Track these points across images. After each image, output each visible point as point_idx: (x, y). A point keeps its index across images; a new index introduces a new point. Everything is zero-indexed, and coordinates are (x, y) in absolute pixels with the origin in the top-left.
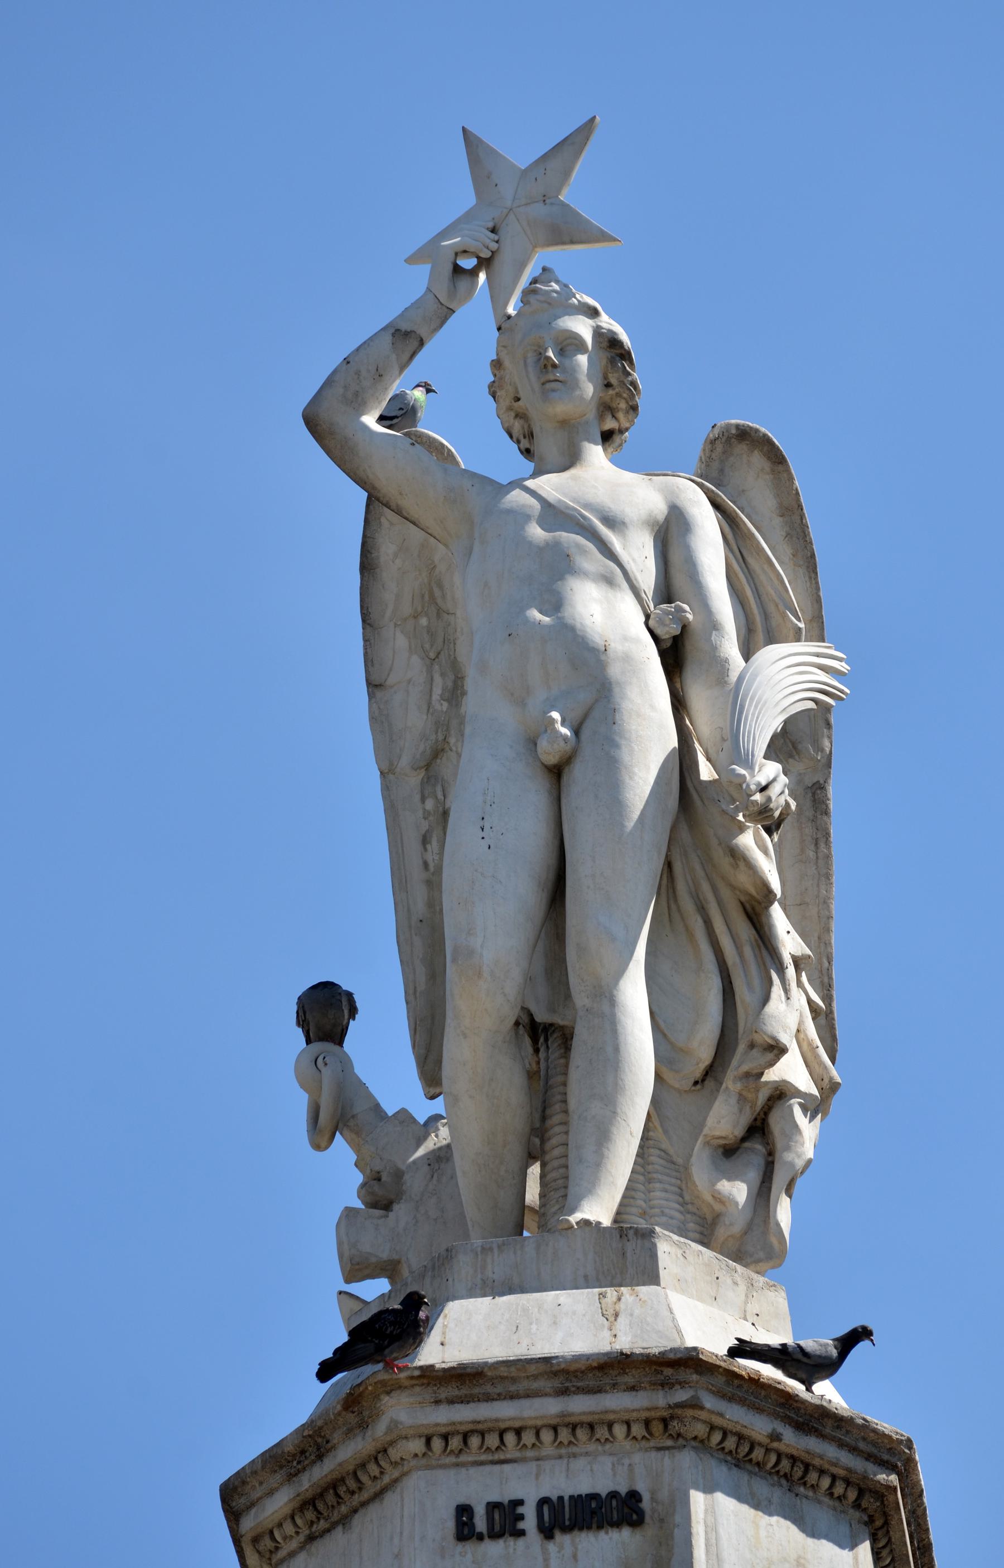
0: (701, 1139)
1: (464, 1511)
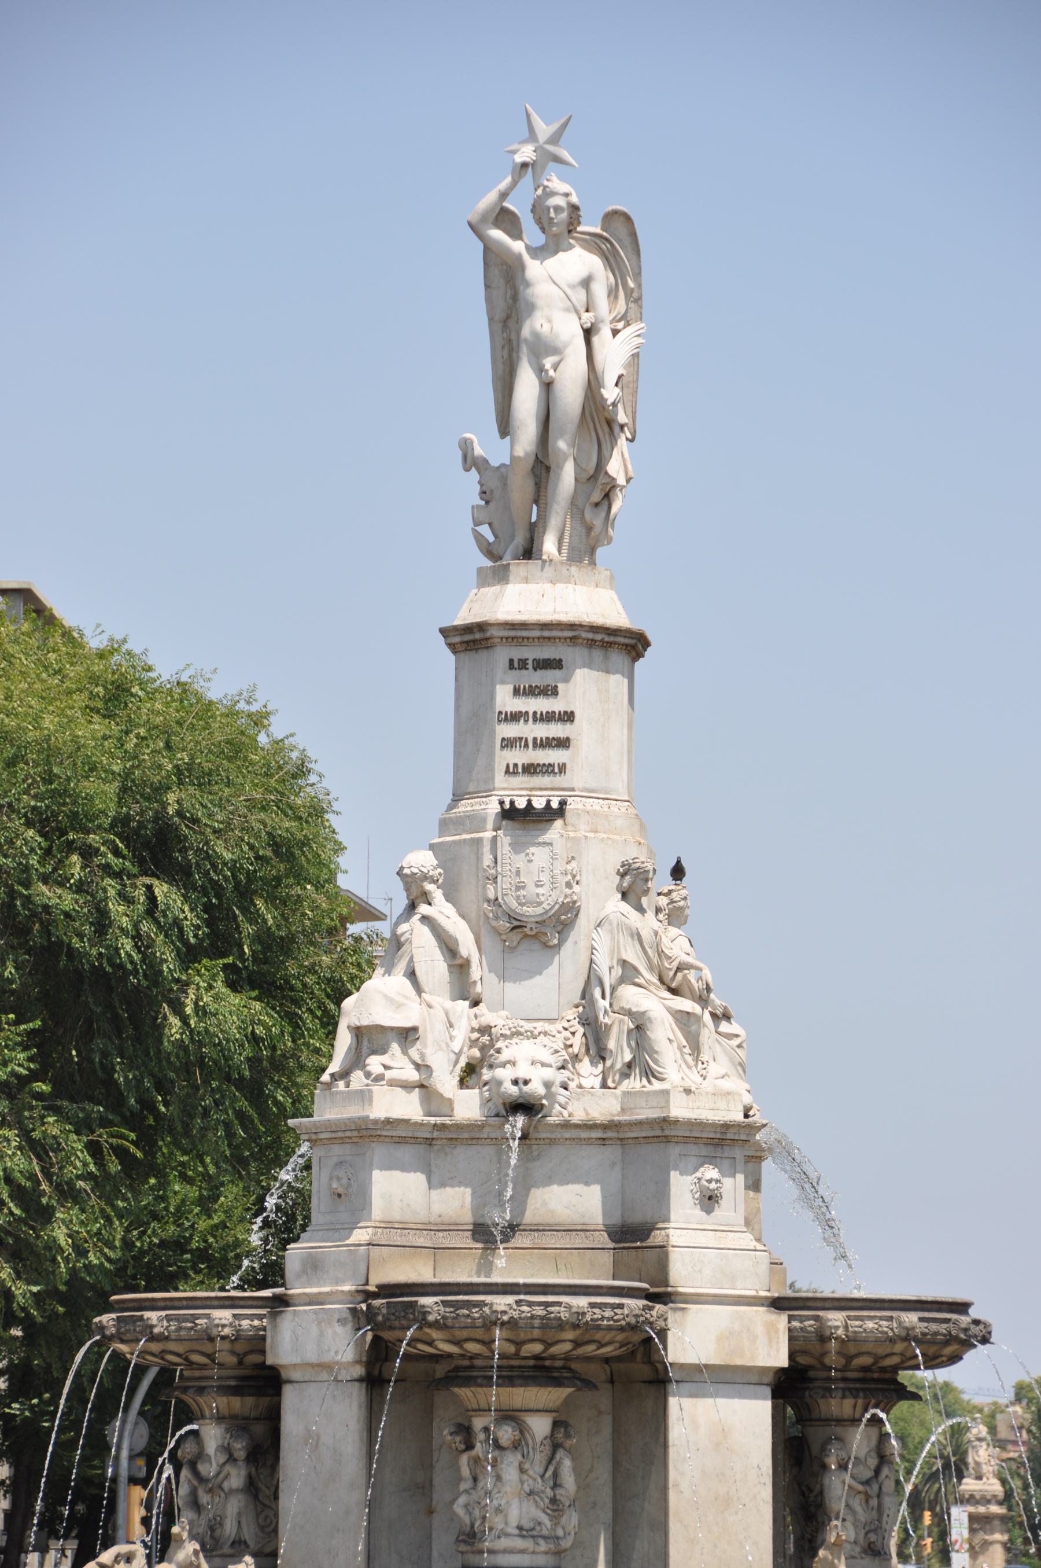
1: (511, 661)
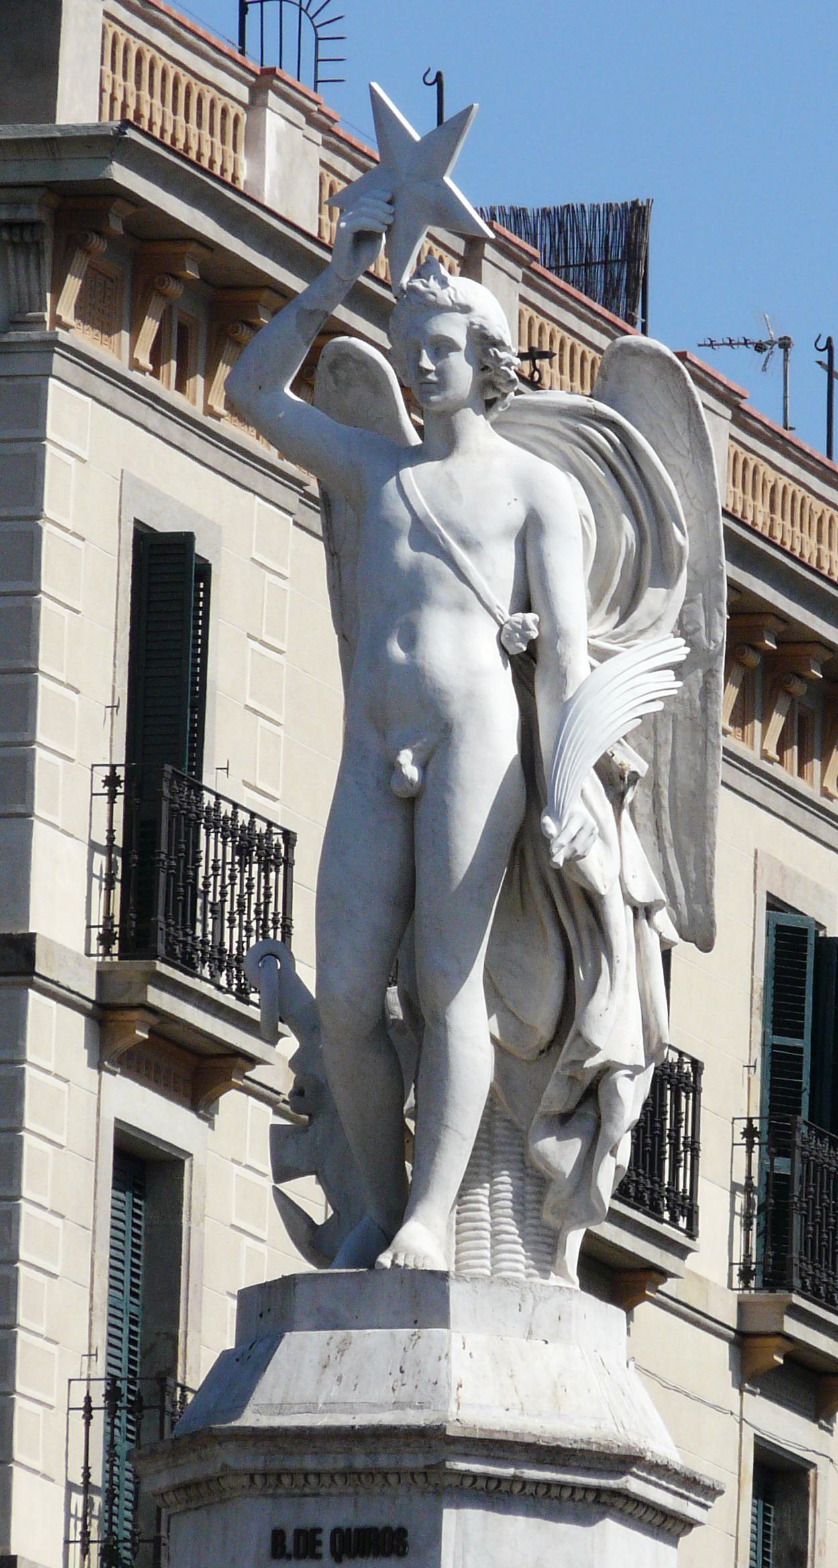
0: (536, 1116)
1: (278, 1536)
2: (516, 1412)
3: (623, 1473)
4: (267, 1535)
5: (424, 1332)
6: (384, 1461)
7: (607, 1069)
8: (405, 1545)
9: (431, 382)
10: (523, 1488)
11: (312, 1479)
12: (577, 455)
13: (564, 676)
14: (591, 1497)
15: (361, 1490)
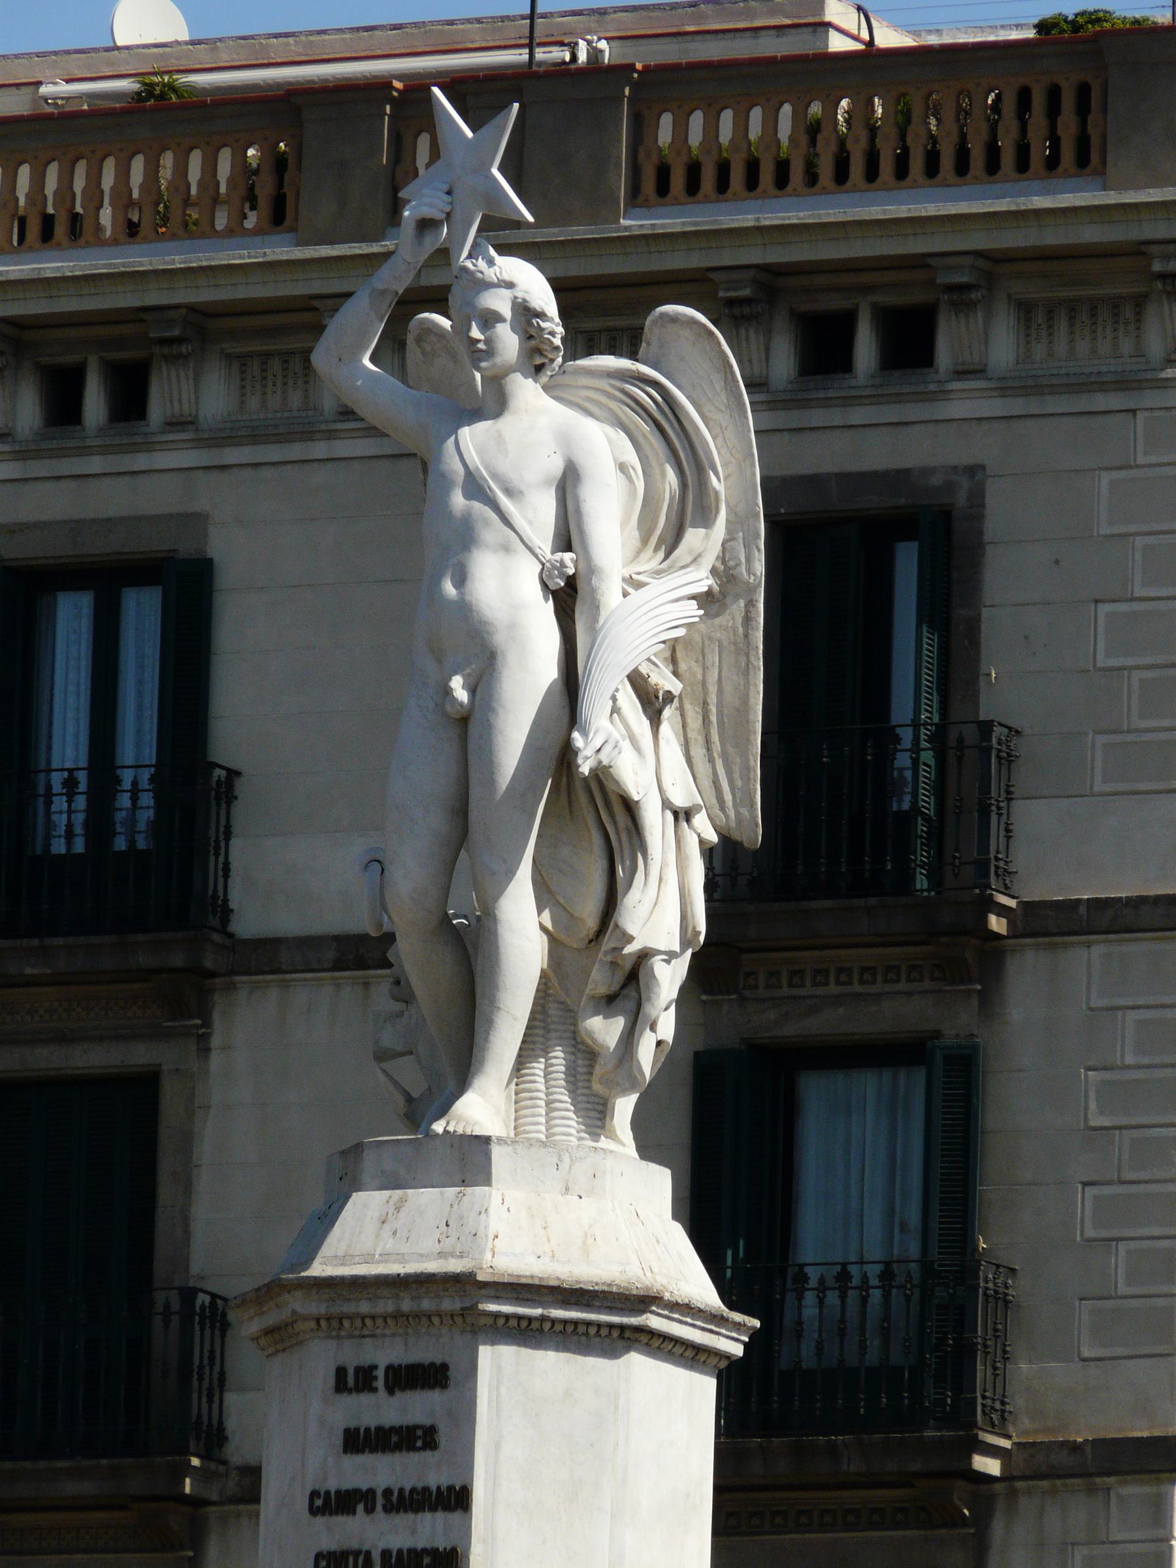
1: (341, 1372)
2: (547, 1259)
3: (644, 1312)
4: (332, 1373)
5: (469, 1190)
6: (426, 1305)
7: (645, 955)
8: (447, 1378)
9: (481, 351)
10: (552, 1326)
11: (368, 1321)
12: (626, 414)
13: (598, 607)
14: (615, 1333)
15: (410, 1331)
